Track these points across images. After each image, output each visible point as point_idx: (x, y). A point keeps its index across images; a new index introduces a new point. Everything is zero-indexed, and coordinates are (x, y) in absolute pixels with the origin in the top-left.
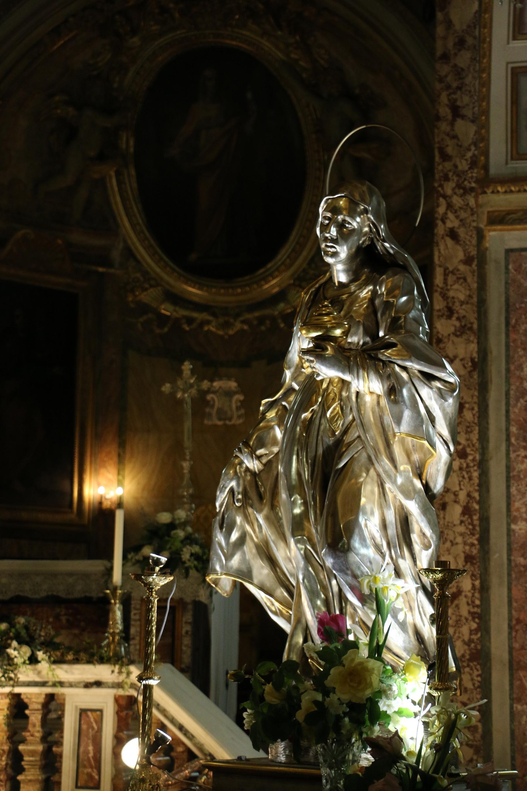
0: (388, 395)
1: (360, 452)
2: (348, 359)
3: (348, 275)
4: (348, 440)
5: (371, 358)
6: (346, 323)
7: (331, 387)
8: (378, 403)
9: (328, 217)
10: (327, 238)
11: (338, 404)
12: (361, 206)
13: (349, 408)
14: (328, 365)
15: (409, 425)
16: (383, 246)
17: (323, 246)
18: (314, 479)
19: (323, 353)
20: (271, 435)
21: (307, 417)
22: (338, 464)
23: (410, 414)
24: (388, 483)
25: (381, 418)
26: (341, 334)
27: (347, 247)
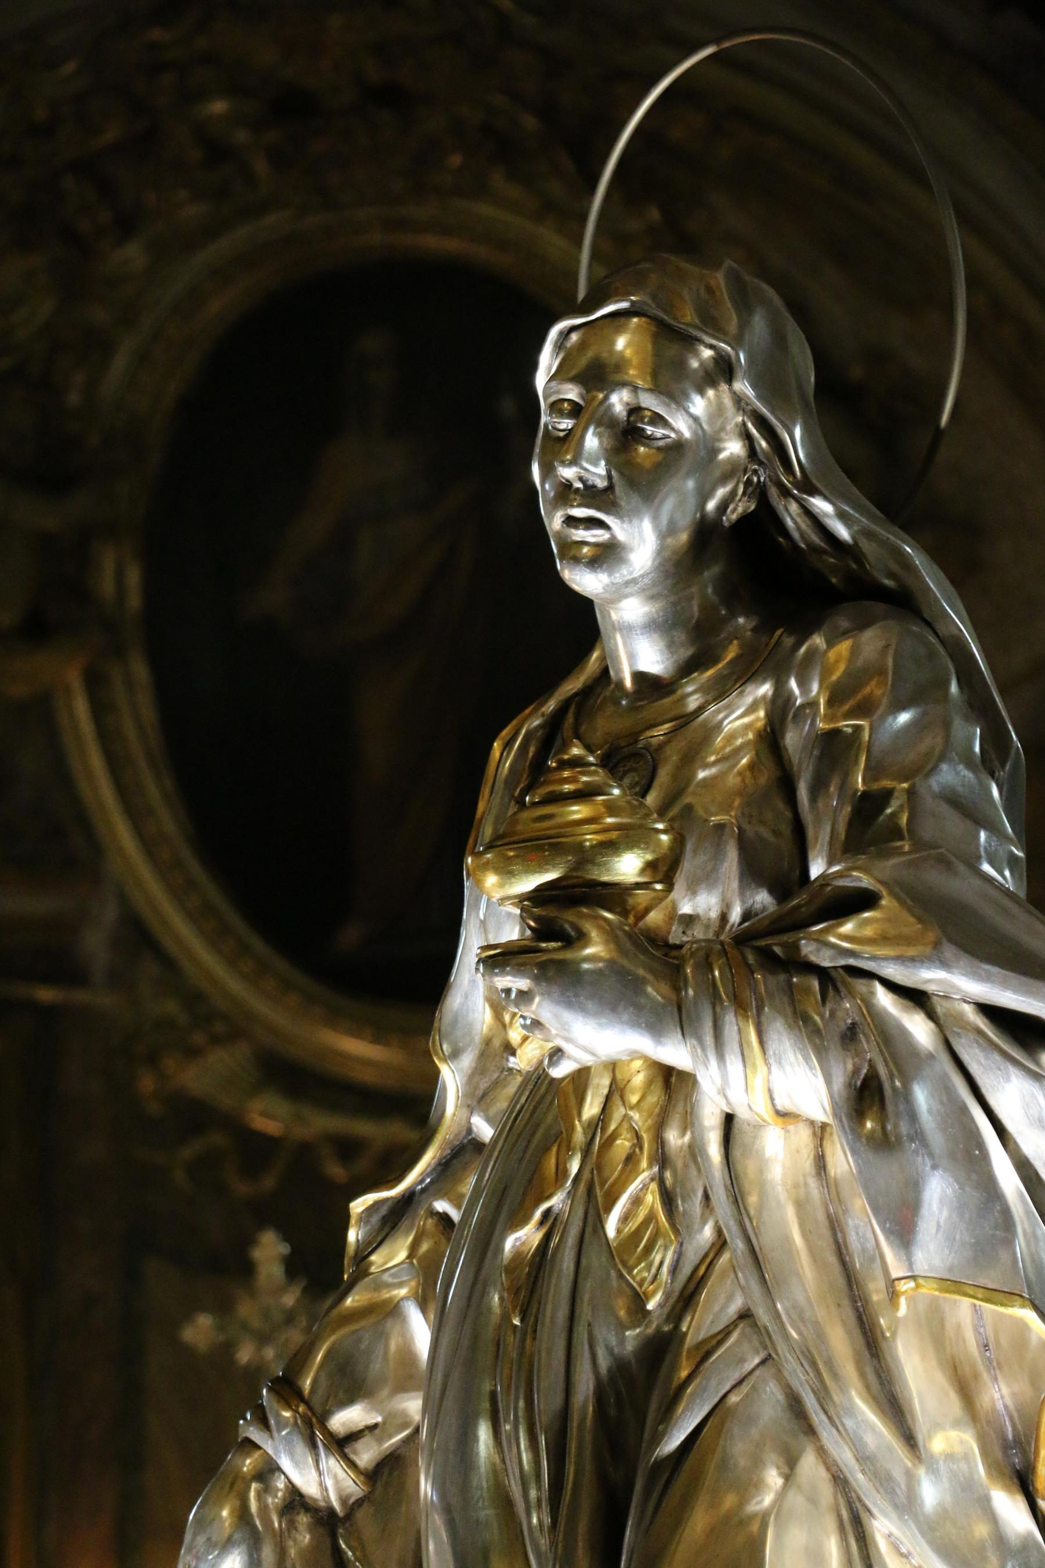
0: (850, 1117)
1: (752, 1379)
2: (674, 976)
3: (671, 646)
4: (699, 1329)
5: (771, 962)
6: (660, 826)
7: (618, 1112)
8: (821, 1163)
10: (567, 486)
11: (652, 1180)
12: (702, 348)
13: (700, 1193)
14: (590, 1005)
15: (950, 1239)
16: (808, 513)
17: (555, 523)
18: (564, 1511)
19: (569, 955)
20: (393, 1346)
21: (525, 1249)
22: (657, 1438)
23: (949, 1191)
24: (885, 1515)
25: (835, 1225)
26: (643, 871)
27: (656, 527)
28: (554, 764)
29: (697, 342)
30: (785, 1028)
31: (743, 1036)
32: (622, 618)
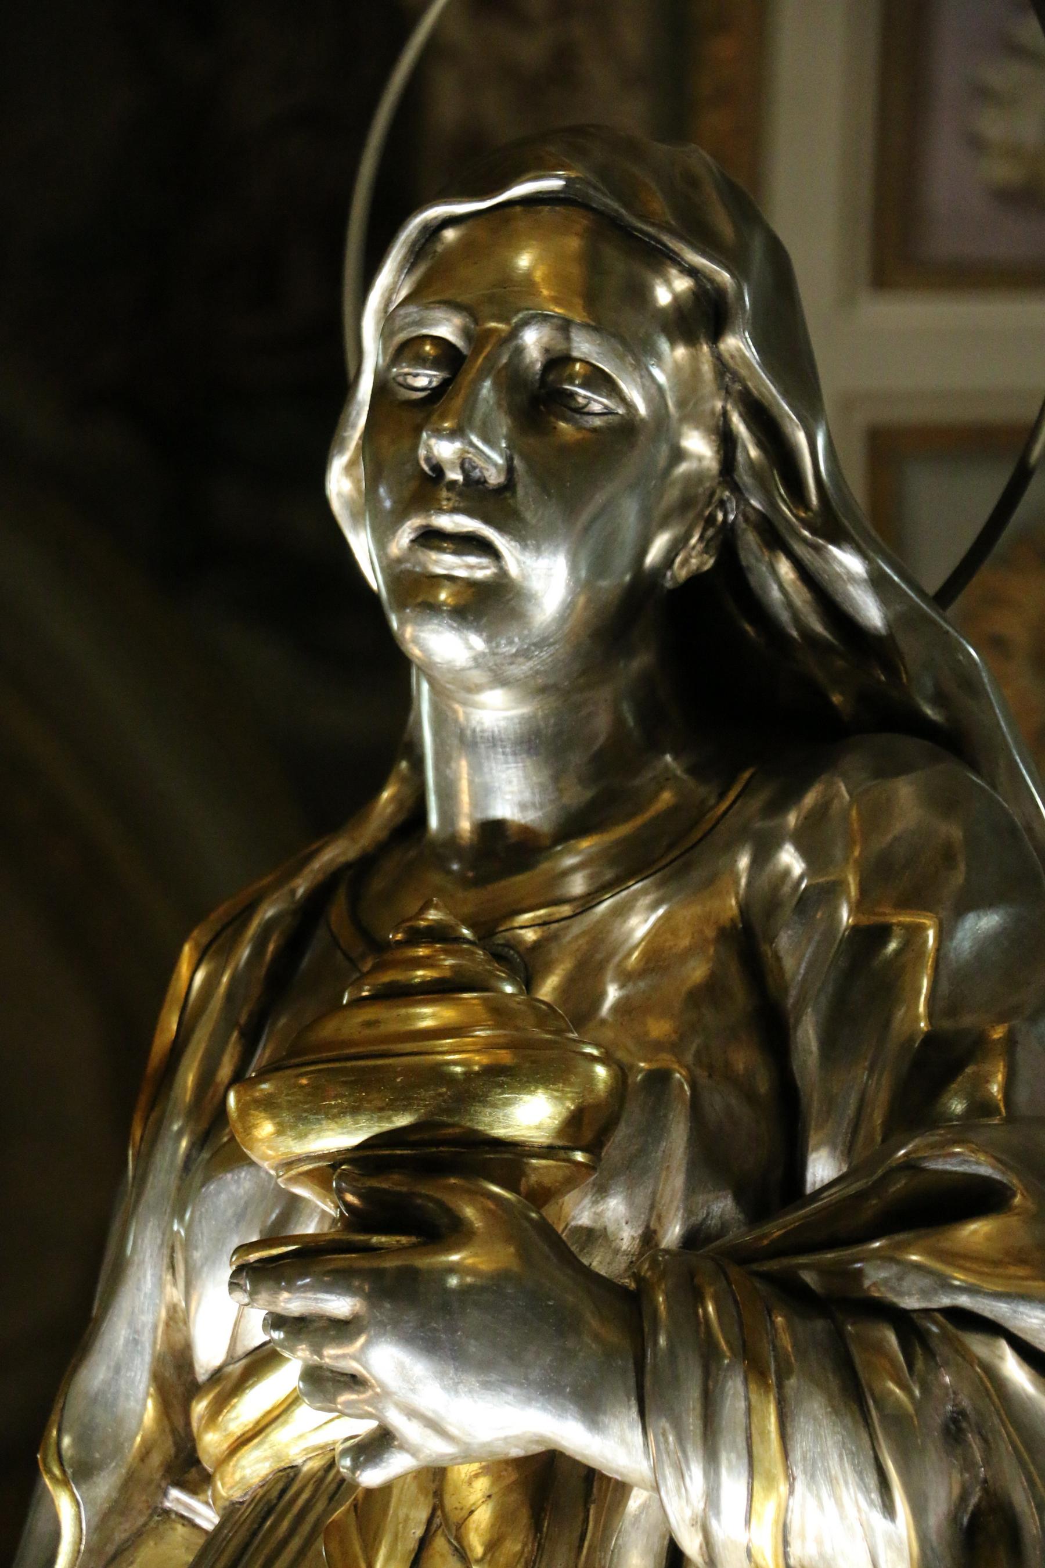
9: (439, 342)
19: (426, 1262)
28: (399, 936)
29: (669, 262)
30: (827, 1413)
31: (755, 1419)
32: (482, 723)
